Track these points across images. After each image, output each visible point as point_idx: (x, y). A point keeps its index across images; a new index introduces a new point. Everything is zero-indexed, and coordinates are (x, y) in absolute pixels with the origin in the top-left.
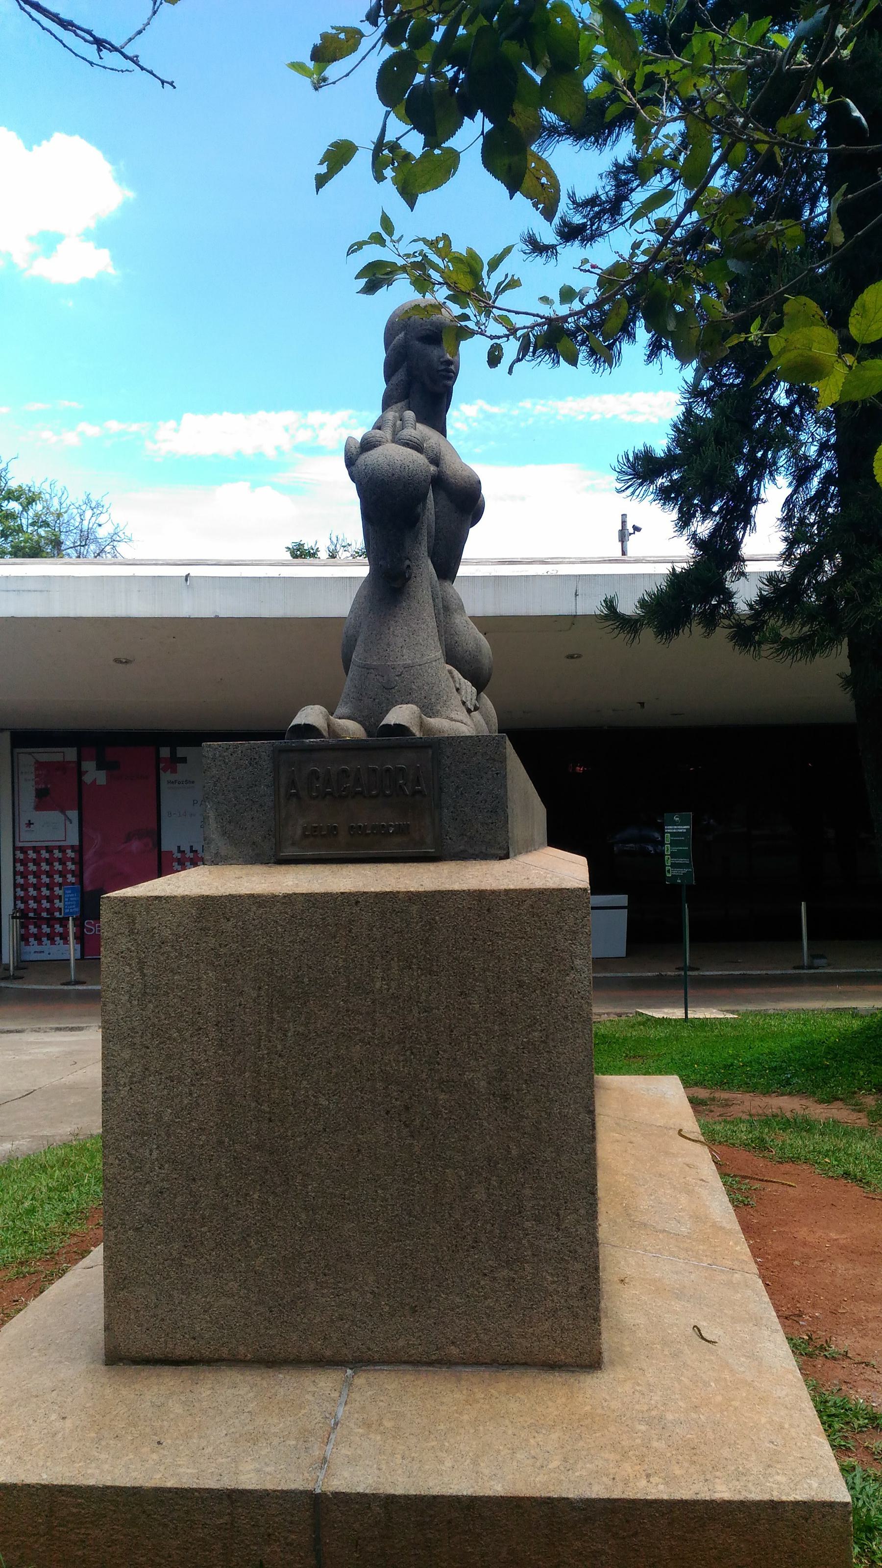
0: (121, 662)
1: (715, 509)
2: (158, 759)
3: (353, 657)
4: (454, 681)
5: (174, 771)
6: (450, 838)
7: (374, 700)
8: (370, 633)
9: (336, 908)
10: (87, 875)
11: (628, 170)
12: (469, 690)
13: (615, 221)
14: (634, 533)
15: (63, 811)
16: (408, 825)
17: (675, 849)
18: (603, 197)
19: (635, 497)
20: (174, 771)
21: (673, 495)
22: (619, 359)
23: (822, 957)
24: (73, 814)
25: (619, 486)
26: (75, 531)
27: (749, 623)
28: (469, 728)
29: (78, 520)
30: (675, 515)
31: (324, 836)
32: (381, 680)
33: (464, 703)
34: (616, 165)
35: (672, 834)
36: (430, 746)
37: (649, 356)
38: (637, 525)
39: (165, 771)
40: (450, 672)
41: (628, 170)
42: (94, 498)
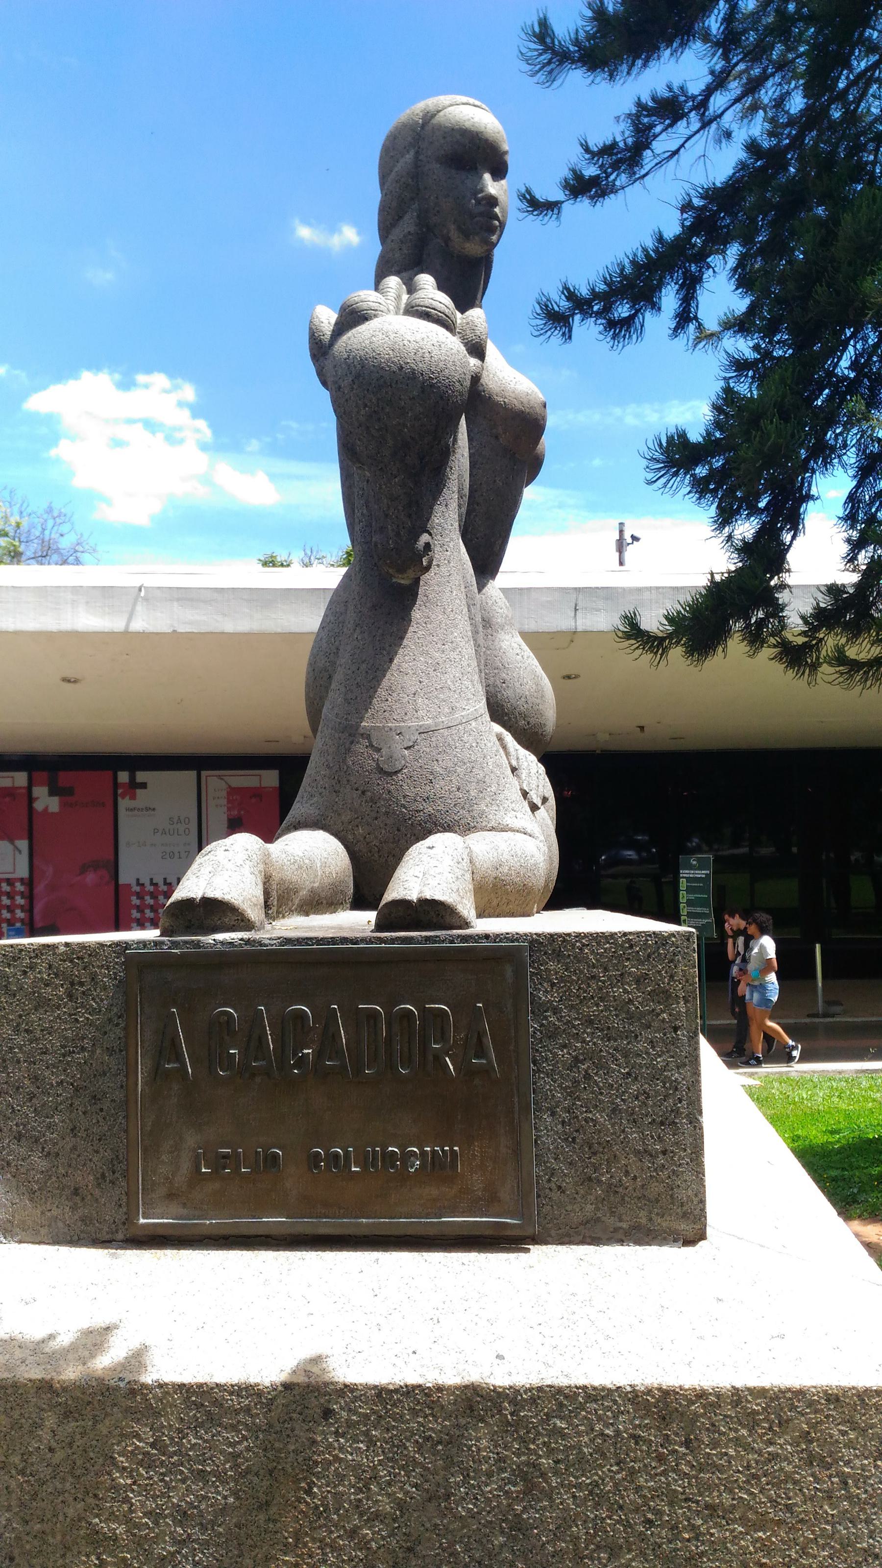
0: (69, 681)
1: (762, 505)
2: (116, 785)
3: (324, 710)
4: (507, 754)
5: (133, 797)
7: (363, 793)
10: (38, 908)
11: (651, 112)
12: (534, 771)
13: (635, 173)
14: (633, 543)
15: (12, 841)
17: (692, 896)
18: (621, 145)
19: (667, 490)
20: (133, 797)
21: (712, 487)
22: (641, 333)
23: (838, 1003)
24: (23, 844)
25: (650, 476)
26: (36, 541)
27: (801, 640)
28: (538, 842)
29: (40, 529)
30: (713, 511)
33: (525, 794)
34: (639, 104)
35: (689, 880)
37: (676, 330)
38: (636, 535)
39: (123, 798)
40: (500, 739)
41: (651, 112)
42: (57, 506)
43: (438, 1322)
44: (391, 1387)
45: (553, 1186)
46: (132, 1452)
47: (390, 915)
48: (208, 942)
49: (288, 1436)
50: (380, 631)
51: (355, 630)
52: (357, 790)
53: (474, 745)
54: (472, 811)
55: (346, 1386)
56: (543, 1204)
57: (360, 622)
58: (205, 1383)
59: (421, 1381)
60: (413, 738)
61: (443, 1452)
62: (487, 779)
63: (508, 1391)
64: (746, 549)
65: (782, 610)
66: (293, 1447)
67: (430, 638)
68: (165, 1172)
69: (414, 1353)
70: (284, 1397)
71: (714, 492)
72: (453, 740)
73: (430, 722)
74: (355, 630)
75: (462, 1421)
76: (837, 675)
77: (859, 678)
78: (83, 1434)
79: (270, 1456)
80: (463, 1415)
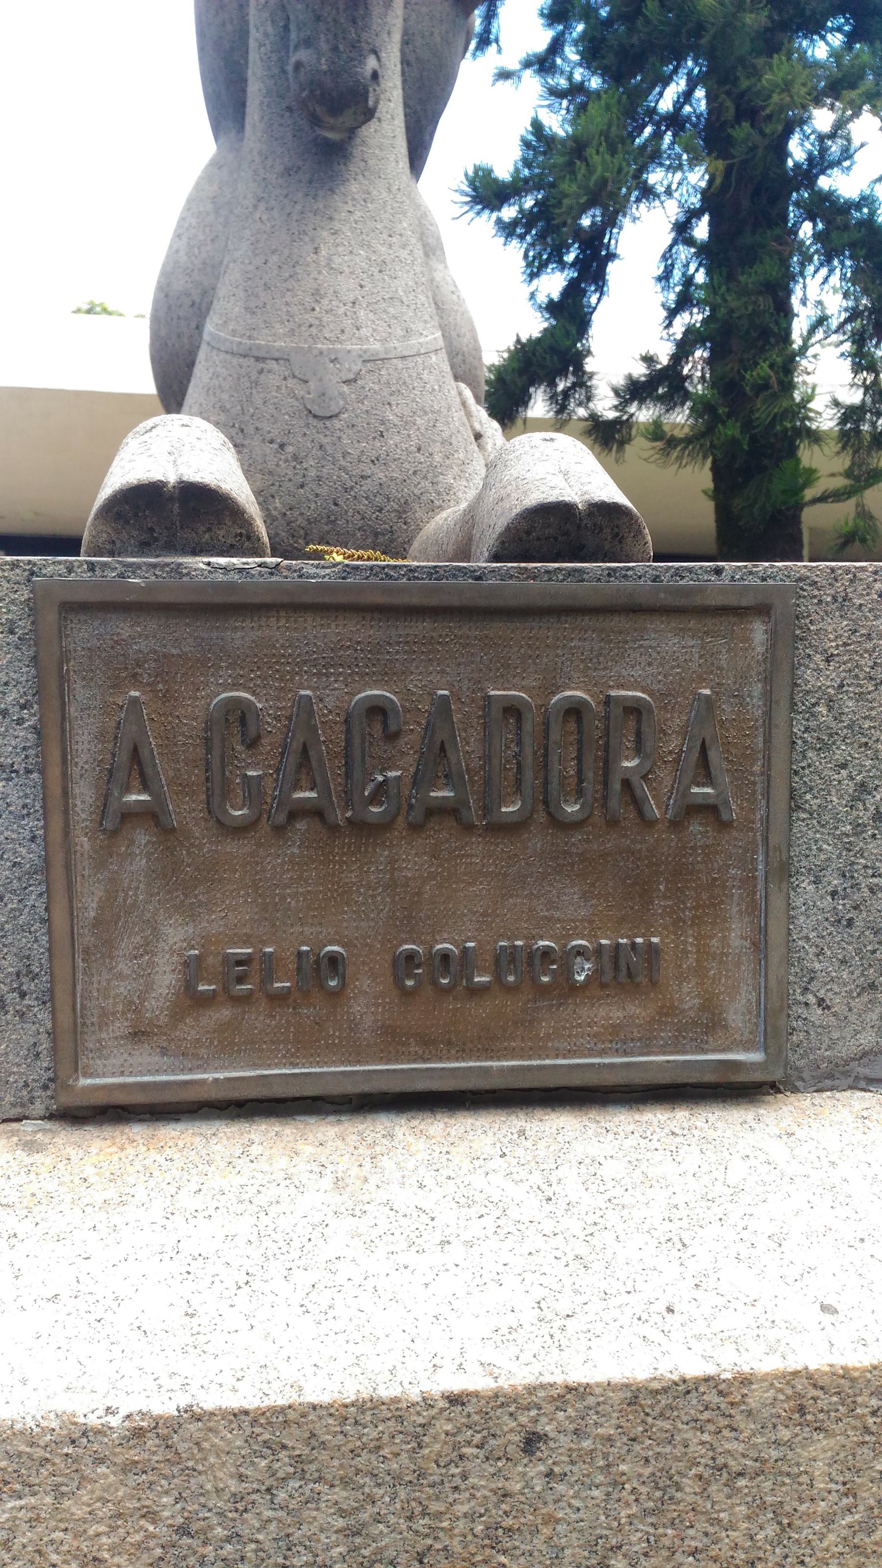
6: (821, 1002)
7: (282, 446)
8: (259, 261)
9: (421, 1474)
16: (652, 951)
31: (279, 999)
32: (300, 391)
36: (762, 610)
43: (684, 1245)
44: (656, 1385)
45: (812, 999)
46: (138, 1545)
47: (528, 533)
48: (195, 566)
49: (456, 1488)
50: (298, 207)
51: (255, 207)
52: (271, 442)
53: (436, 387)
54: (437, 483)
55: (569, 1389)
56: (794, 1029)
57: (265, 195)
58: (290, 1407)
59: (711, 1370)
60: (355, 368)
61: (746, 1491)
62: (453, 441)
63: (869, 1375)
64: (552, 308)
65: (590, 378)
66: (465, 1508)
67: (371, 224)
68: (126, 993)
69: (670, 1310)
70: (449, 1420)
71: (522, 237)
72: (410, 376)
73: (377, 346)
74: (255, 207)
75: (785, 1434)
76: (652, 452)
77: (675, 454)
78: (34, 1522)
79: (421, 1529)
80: (786, 1423)
